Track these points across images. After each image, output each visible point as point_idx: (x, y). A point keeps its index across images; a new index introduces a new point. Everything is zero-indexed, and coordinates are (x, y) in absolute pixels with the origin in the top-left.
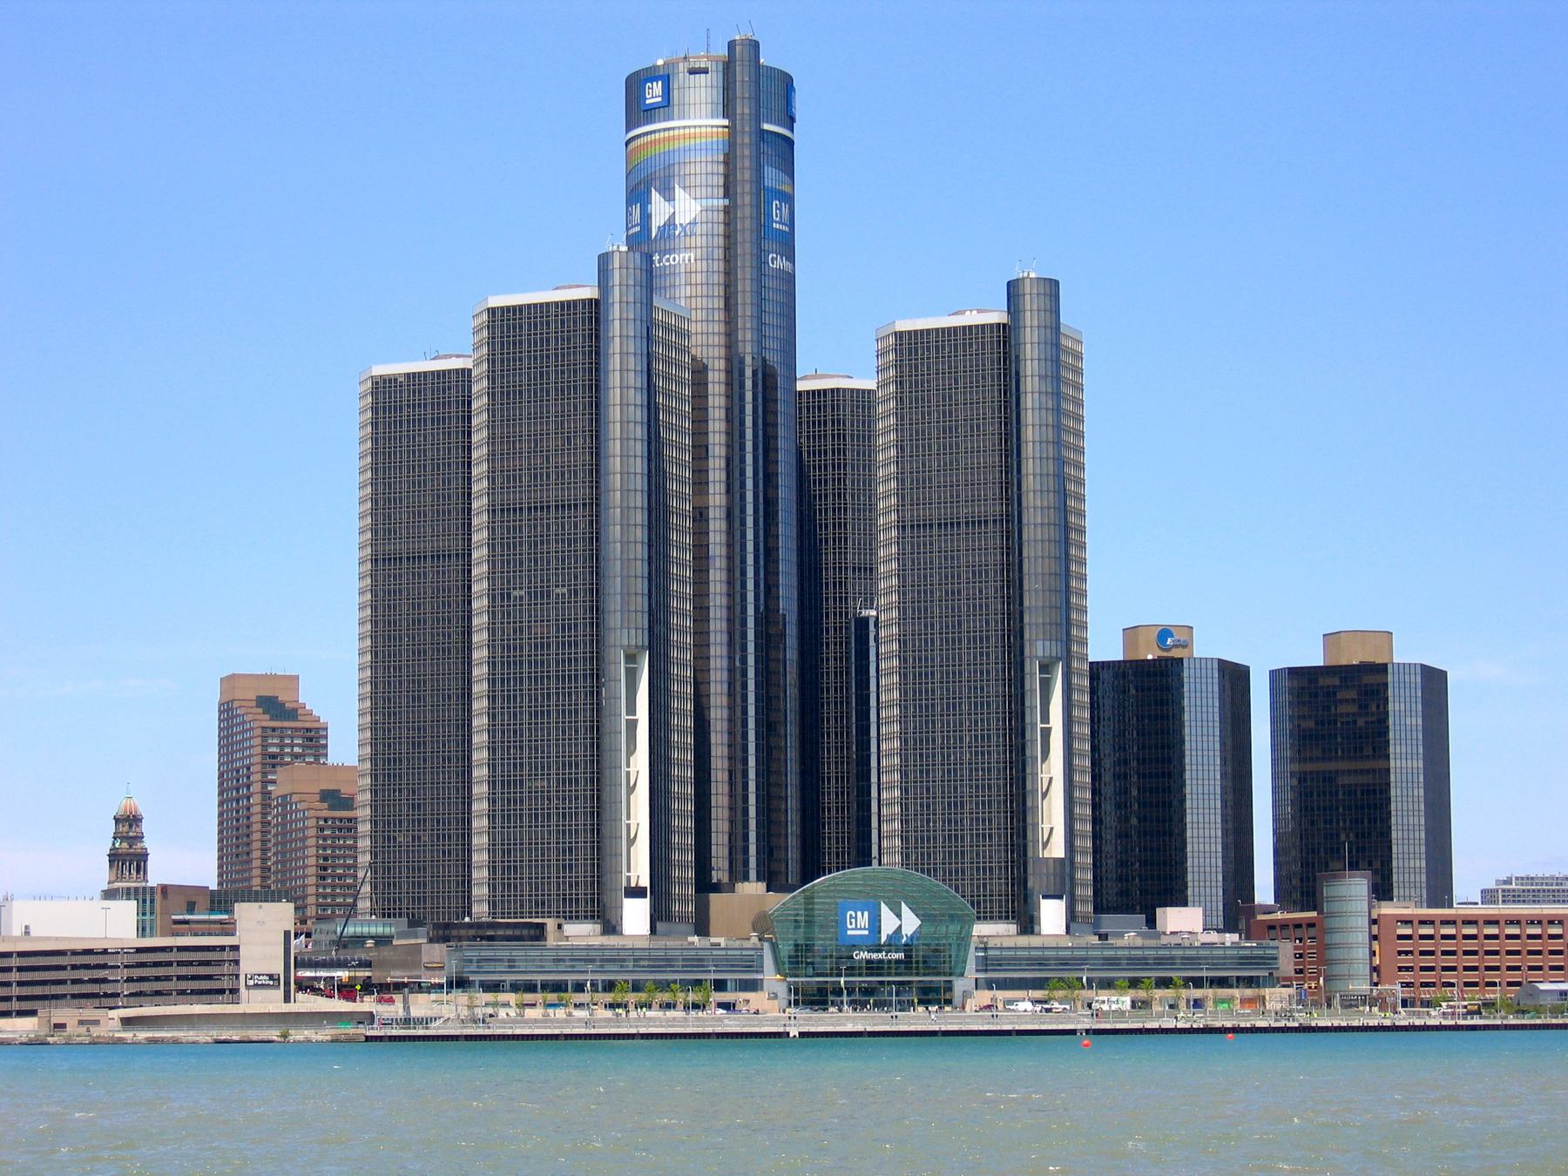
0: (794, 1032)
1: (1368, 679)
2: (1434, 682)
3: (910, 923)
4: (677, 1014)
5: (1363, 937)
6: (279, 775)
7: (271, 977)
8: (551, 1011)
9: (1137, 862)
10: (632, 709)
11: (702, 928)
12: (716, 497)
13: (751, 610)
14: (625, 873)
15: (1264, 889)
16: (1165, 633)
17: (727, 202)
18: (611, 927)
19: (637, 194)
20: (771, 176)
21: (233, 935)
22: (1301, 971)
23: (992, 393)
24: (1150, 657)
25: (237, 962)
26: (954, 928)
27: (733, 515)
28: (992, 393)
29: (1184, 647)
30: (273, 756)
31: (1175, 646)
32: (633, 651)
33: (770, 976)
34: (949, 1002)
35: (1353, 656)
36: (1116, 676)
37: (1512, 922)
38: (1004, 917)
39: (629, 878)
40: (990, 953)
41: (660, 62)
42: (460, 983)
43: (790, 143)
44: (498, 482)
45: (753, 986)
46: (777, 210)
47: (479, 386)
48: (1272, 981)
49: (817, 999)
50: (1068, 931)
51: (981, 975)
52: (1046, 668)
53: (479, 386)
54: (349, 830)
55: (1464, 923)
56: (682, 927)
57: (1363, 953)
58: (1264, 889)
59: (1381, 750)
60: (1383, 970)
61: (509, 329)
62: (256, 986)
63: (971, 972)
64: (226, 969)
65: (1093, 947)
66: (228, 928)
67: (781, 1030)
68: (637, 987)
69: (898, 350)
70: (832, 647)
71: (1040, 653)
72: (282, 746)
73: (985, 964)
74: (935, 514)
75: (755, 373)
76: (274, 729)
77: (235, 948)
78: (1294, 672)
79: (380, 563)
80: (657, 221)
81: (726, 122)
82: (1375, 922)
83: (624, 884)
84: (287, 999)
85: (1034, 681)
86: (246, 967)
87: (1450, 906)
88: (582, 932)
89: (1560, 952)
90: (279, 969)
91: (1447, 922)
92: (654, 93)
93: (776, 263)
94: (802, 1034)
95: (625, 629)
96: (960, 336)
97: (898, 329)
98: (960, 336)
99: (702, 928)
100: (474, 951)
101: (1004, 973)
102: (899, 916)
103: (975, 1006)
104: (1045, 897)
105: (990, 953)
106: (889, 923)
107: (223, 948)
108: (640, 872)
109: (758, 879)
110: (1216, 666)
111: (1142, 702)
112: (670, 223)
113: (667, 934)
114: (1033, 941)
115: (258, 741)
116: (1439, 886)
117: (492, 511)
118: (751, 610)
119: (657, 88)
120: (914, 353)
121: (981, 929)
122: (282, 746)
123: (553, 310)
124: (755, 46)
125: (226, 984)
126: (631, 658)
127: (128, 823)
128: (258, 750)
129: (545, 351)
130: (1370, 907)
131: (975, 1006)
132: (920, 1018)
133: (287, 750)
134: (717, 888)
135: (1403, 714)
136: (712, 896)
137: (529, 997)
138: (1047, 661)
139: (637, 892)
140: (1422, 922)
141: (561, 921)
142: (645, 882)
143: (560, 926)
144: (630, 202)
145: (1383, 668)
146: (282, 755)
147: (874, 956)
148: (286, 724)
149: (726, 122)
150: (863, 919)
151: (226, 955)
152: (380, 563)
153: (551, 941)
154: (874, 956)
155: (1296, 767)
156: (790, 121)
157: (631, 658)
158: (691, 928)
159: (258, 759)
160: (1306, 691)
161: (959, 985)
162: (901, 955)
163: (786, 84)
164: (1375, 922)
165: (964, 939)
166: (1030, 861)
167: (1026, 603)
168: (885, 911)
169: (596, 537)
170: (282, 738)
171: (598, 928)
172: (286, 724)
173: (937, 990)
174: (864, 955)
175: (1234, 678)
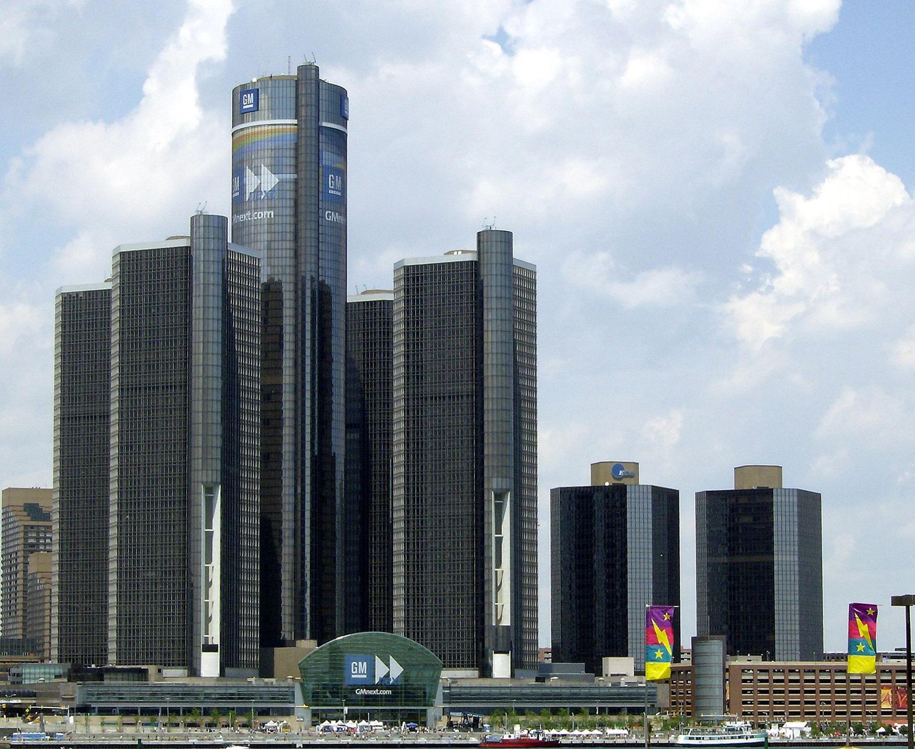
1: (759, 500)
2: (809, 504)
3: (396, 670)
4: (180, 730)
5: (718, 681)
6: (32, 559)
9: (594, 624)
10: (209, 524)
11: (266, 670)
12: (287, 378)
13: (308, 454)
14: (203, 635)
16: (618, 466)
17: (296, 176)
18: (194, 672)
19: (238, 172)
20: (328, 158)
22: (674, 703)
23: (474, 308)
24: (607, 484)
26: (428, 673)
27: (298, 390)
28: (474, 308)
29: (631, 476)
30: (32, 545)
31: (625, 476)
33: (299, 705)
34: (424, 724)
36: (607, 496)
37: (809, 671)
38: (470, 666)
39: (207, 639)
40: (453, 690)
41: (255, 80)
42: (84, 709)
43: (343, 136)
44: (125, 370)
45: (288, 712)
46: (332, 181)
48: (653, 709)
50: (513, 675)
51: (447, 706)
52: (500, 496)
55: (897, 671)
56: (250, 671)
57: (718, 692)
58: (545, 639)
59: (769, 549)
61: (132, 264)
63: (439, 703)
65: (532, 687)
68: (207, 712)
69: (407, 279)
70: (378, 477)
71: (495, 487)
72: (38, 538)
75: (313, 292)
76: (32, 527)
78: (709, 493)
79: (66, 421)
80: (250, 188)
81: (295, 122)
82: (727, 670)
83: (202, 642)
85: (491, 506)
88: (175, 675)
93: (331, 217)
94: (305, 746)
95: (205, 469)
96: (446, 269)
98: (446, 269)
99: (266, 670)
100: (93, 687)
102: (388, 665)
105: (453, 690)
106: (381, 670)
108: (215, 634)
109: (312, 638)
111: (596, 514)
112: (258, 191)
113: (232, 677)
115: (22, 535)
117: (121, 389)
118: (308, 454)
119: (251, 98)
120: (415, 278)
121: (446, 674)
122: (38, 538)
123: (161, 253)
126: (209, 490)
128: (21, 541)
130: (725, 660)
133: (42, 541)
134: (283, 644)
136: (278, 651)
137: (131, 719)
138: (499, 492)
139: (211, 648)
140: (822, 671)
141: (161, 667)
142: (217, 641)
143: (160, 671)
144: (234, 175)
145: (768, 492)
146: (38, 545)
147: (370, 692)
148: (41, 523)
149: (295, 122)
150: (363, 667)
152: (66, 421)
153: (153, 680)
154: (370, 692)
156: (344, 119)
157: (209, 490)
158: (257, 672)
159: (21, 547)
160: (712, 501)
161: (431, 712)
162: (390, 692)
163: (340, 95)
164: (727, 670)
165: (436, 680)
166: (486, 628)
167: (486, 452)
168: (378, 662)
169: (187, 408)
170: (38, 533)
171: (476, 673)
172: (41, 523)
174: (364, 692)
175: (666, 501)
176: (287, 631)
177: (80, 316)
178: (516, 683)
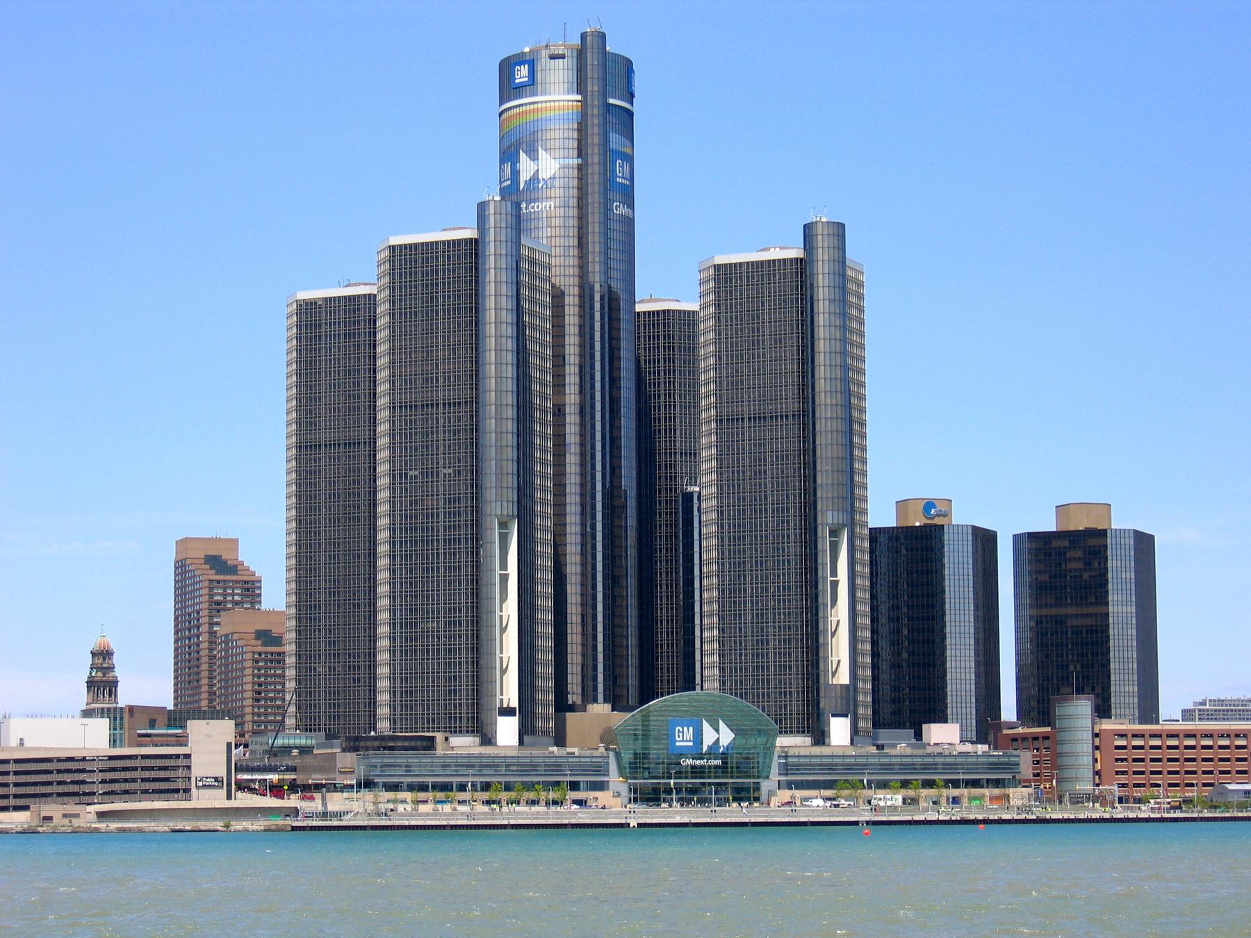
0: (633, 823)
1: (1092, 542)
2: (1144, 544)
3: (726, 736)
4: (540, 808)
5: (1087, 748)
6: (223, 618)
7: (216, 779)
8: (439, 806)
9: (907, 687)
10: (504, 565)
11: (560, 740)
12: (572, 397)
13: (599, 487)
14: (499, 697)
15: (1009, 709)
16: (929, 505)
17: (580, 161)
18: (488, 739)
19: (509, 155)
20: (615, 140)
21: (186, 745)
22: (1038, 775)
23: (791, 314)
24: (917, 524)
25: (189, 767)
26: (761, 740)
27: (585, 411)
28: (791, 314)
29: (945, 516)
30: (218, 603)
31: (938, 515)
32: (505, 519)
33: (614, 778)
34: (757, 799)
35: (1080, 523)
36: (890, 539)
37: (1206, 736)
38: (801, 731)
39: (502, 701)
40: (790, 760)
41: (527, 50)
42: (367, 784)
43: (630, 114)
44: (397, 384)
45: (601, 786)
46: (620, 168)
47: (382, 308)
48: (1015, 782)
49: (651, 797)
50: (852, 742)
51: (783, 778)
52: (834, 533)
53: (382, 308)
54: (279, 662)
56: (544, 739)
57: (1087, 760)
58: (1009, 709)
59: (1102, 599)
60: (1103, 774)
61: (406, 262)
62: (204, 786)
63: (775, 775)
64: (180, 773)
65: (872, 756)
66: (182, 740)
67: (623, 821)
68: (508, 787)
69: (717, 279)
70: (664, 516)
71: (830, 521)
72: (225, 595)
73: (786, 769)
74: (746, 410)
75: (602, 298)
76: (218, 582)
77: (188, 756)
78: (1032, 536)
79: (303, 449)
80: (524, 176)
81: (579, 97)
82: (1097, 735)
83: (498, 705)
84: (229, 797)
85: (825, 544)
86: (196, 771)
87: (1157, 723)
88: (464, 744)
90: (222, 773)
91: (1154, 735)
92: (522, 74)
93: (619, 209)
94: (640, 825)
95: (498, 501)
96: (766, 268)
97: (717, 262)
98: (766, 268)
99: (560, 740)
100: (378, 759)
101: (801, 776)
102: (717, 731)
103: (778, 803)
104: (834, 715)
105: (790, 760)
106: (709, 736)
107: (178, 756)
108: (511, 696)
109: (605, 701)
110: (970, 531)
111: (911, 560)
112: (535, 178)
113: (532, 745)
114: (824, 750)
115: (206, 591)
116: (1148, 706)
117: (393, 408)
118: (599, 487)
119: (524, 70)
120: (729, 282)
121: (783, 741)
122: (225, 595)
123: (441, 247)
124: (602, 37)
125: (180, 785)
126: (503, 525)
127: (102, 656)
128: (206, 598)
129: (435, 280)
130: (1093, 724)
131: (778, 803)
132: (734, 812)
133: (229, 598)
134: (572, 708)
135: (1120, 570)
136: (568, 715)
137: (422, 795)
138: (835, 527)
139: (508, 712)
140: (1135, 736)
141: (448, 734)
142: (515, 703)
143: (446, 739)
144: (502, 161)
145: (1103, 533)
146: (225, 602)
147: (698, 762)
148: (228, 577)
149: (579, 97)
150: (689, 733)
151: (180, 762)
152: (303, 449)
153: (440, 750)
154: (698, 762)
155: (1034, 612)
156: (630, 97)
157: (503, 525)
158: (551, 740)
159: (206, 605)
160: (1042, 551)
161: (765, 786)
162: (719, 762)
163: (627, 67)
164: (1097, 735)
165: (769, 749)
166: (822, 687)
167: (819, 481)
168: (706, 727)
169: (475, 428)
170: (225, 589)
171: (477, 740)
172: (228, 577)
173: (747, 790)
174: (690, 762)
175: (985, 541)
176: (574, 697)
177: (328, 336)
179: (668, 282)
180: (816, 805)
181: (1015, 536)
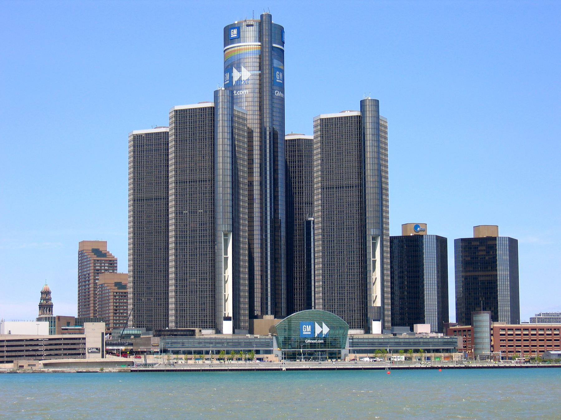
0: (284, 369)
1: (490, 243)
2: (513, 244)
3: (326, 330)
4: (242, 362)
5: (488, 335)
6: (100, 277)
7: (97, 349)
8: (197, 361)
9: (407, 308)
10: (226, 253)
11: (251, 332)
12: (256, 178)
13: (269, 218)
14: (224, 312)
15: (452, 317)
16: (417, 226)
17: (260, 72)
18: (219, 331)
19: (228, 69)
20: (276, 63)
21: (83, 334)
22: (465, 347)
23: (355, 141)
24: (411, 235)
25: (85, 344)
26: (341, 331)
27: (262, 184)
28: (355, 141)
29: (424, 231)
30: (98, 270)
31: (421, 231)
32: (226, 232)
33: (275, 349)
34: (339, 358)
35: (484, 234)
36: (399, 241)
37: (541, 329)
38: (359, 327)
39: (225, 314)
40: (354, 340)
41: (236, 22)
42: (165, 351)
43: (283, 51)
44: (178, 172)
45: (269, 352)
46: (278, 75)
47: (171, 138)
48: (455, 350)
49: (292, 357)
50: (382, 332)
51: (351, 348)
52: (374, 239)
53: (171, 138)
54: (125, 296)
55: (524, 329)
56: (244, 331)
57: (488, 340)
58: (452, 317)
59: (494, 268)
60: (495, 347)
61: (182, 117)
62: (92, 352)
63: (347, 347)
64: (81, 346)
65: (391, 338)
66: (81, 332)
67: (279, 368)
68: (228, 353)
69: (321, 125)
70: (298, 231)
71: (372, 233)
72: (101, 266)
73: (352, 344)
74: (335, 183)
75: (270, 133)
76: (98, 261)
77: (84, 339)
78: (463, 240)
79: (136, 201)
80: (235, 79)
81: (260, 44)
82: (492, 329)
83: (223, 316)
84: (103, 357)
85: (370, 243)
86: (88, 345)
87: (519, 324)
88: (208, 333)
89: (558, 340)
90: (100, 346)
91: (518, 329)
92: (234, 33)
93: (278, 94)
94: (287, 369)
95: (224, 225)
96: (343, 120)
97: (321, 117)
98: (343, 120)
99: (251, 332)
100: (170, 340)
101: (359, 348)
102: (322, 327)
103: (349, 359)
104: (374, 320)
105: (354, 340)
106: (318, 330)
107: (80, 339)
108: (229, 312)
109: (271, 314)
110: (435, 238)
111: (408, 251)
112: (240, 80)
113: (239, 334)
114: (369, 336)
115: (92, 265)
116: (515, 316)
117: (176, 183)
118: (269, 218)
119: (235, 31)
120: (327, 126)
121: (351, 332)
122: (101, 266)
123: (198, 111)
124: (270, 16)
125: (81, 351)
126: (226, 235)
127: (46, 294)
128: (92, 268)
129: (195, 125)
130: (490, 324)
131: (349, 359)
132: (329, 364)
133: (103, 268)
134: (256, 317)
135: (502, 255)
136: (255, 320)
137: (189, 356)
138: (374, 236)
139: (228, 319)
140: (509, 329)
141: (201, 329)
142: (231, 315)
143: (200, 331)
144: (225, 72)
145: (495, 239)
146: (101, 270)
147: (313, 341)
148: (102, 259)
149: (260, 44)
150: (309, 328)
151: (81, 341)
152: (136, 201)
153: (197, 336)
154: (313, 341)
155: (464, 274)
156: (283, 43)
157: (226, 235)
158: (247, 331)
159: (92, 271)
160: (467, 247)
161: (343, 352)
162: (322, 341)
163: (281, 30)
164: (492, 329)
165: (345, 335)
166: (369, 308)
167: (367, 215)
168: (317, 325)
169: (213, 192)
170: (101, 264)
171: (214, 331)
172: (102, 259)
173: (335, 354)
174: (309, 341)
175: (442, 242)
177: (147, 151)
178: (236, 337)
179: (299, 126)
180: (366, 360)
181: (455, 240)
